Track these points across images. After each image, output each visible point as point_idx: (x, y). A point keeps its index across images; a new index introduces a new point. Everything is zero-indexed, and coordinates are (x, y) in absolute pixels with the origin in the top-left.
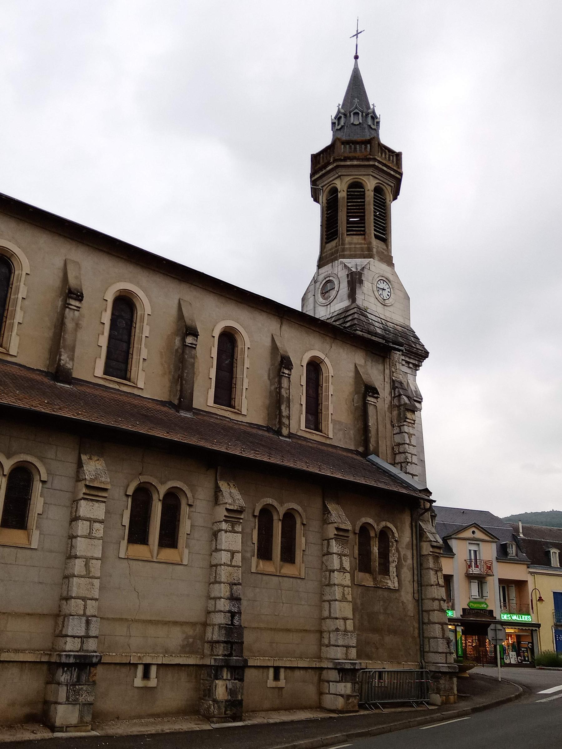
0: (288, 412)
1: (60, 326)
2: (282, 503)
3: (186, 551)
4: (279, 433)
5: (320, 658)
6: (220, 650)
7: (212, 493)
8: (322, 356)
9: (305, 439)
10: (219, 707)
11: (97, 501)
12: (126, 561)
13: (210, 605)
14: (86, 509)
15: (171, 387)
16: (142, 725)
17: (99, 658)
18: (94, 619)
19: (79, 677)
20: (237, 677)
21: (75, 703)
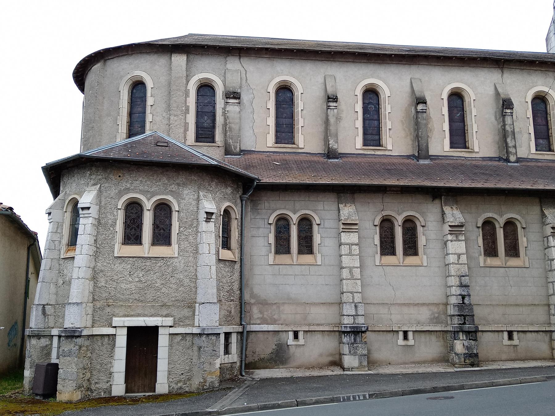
0: (514, 143)
1: (327, 122)
2: (501, 216)
3: (425, 257)
4: (507, 160)
5: (550, 324)
6: (456, 320)
7: (440, 215)
8: (546, 89)
9: (537, 160)
10: (459, 357)
11: (352, 232)
12: (381, 267)
13: (448, 291)
14: (345, 238)
15: (413, 144)
16: (405, 368)
17: (366, 328)
18: (361, 304)
19: (355, 339)
20: (471, 338)
21: (355, 354)
